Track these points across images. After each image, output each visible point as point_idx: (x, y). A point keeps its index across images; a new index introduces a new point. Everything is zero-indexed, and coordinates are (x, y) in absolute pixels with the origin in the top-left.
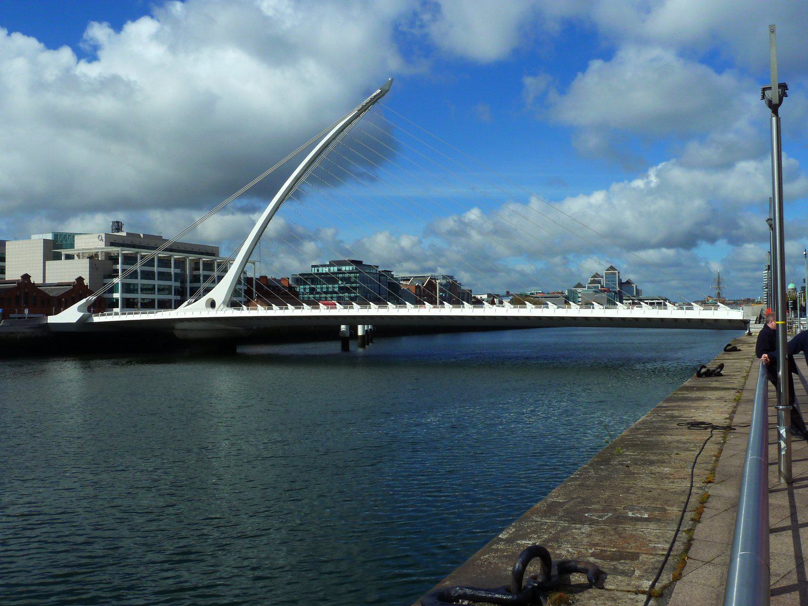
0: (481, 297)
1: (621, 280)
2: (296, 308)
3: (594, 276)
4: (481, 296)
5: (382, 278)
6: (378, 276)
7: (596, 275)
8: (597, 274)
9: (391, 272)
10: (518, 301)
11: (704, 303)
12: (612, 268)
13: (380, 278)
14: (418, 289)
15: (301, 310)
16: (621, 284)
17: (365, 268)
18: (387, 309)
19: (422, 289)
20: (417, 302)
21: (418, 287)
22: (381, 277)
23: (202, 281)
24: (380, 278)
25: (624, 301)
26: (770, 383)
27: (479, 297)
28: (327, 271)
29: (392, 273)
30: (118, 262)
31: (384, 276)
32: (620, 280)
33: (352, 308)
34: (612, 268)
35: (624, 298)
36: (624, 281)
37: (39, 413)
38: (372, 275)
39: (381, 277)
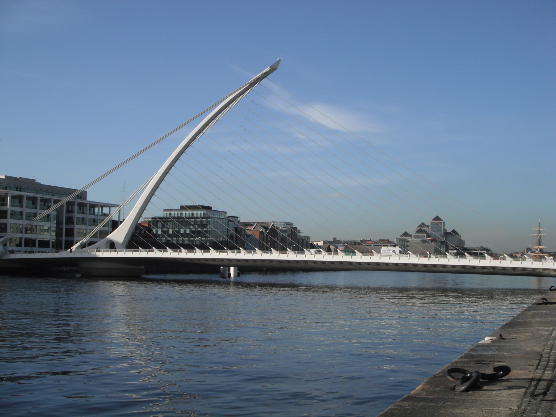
0: (317, 244)
1: (446, 230)
2: (189, 252)
3: (420, 226)
4: (317, 243)
5: (230, 223)
6: (227, 222)
7: (423, 225)
8: (423, 224)
9: (237, 217)
10: (348, 250)
11: (513, 256)
12: (437, 218)
13: (228, 223)
14: (262, 235)
15: (139, 253)
16: (446, 234)
17: (215, 213)
18: (287, 255)
19: (265, 235)
20: (265, 248)
21: (262, 233)
22: (229, 222)
23: (75, 223)
24: (228, 223)
25: (450, 251)
26: (207, 415)
27: (315, 243)
28: (168, 216)
29: (239, 219)
30: (7, 204)
31: (231, 221)
32: (445, 230)
33: (239, 252)
34: (437, 218)
35: (450, 248)
36: (449, 231)
37: (335, 315)
38: (222, 221)
39: (229, 222)
